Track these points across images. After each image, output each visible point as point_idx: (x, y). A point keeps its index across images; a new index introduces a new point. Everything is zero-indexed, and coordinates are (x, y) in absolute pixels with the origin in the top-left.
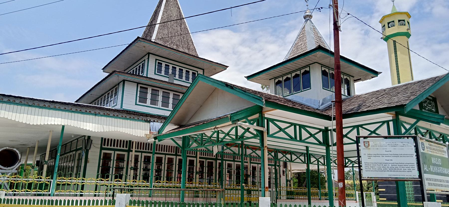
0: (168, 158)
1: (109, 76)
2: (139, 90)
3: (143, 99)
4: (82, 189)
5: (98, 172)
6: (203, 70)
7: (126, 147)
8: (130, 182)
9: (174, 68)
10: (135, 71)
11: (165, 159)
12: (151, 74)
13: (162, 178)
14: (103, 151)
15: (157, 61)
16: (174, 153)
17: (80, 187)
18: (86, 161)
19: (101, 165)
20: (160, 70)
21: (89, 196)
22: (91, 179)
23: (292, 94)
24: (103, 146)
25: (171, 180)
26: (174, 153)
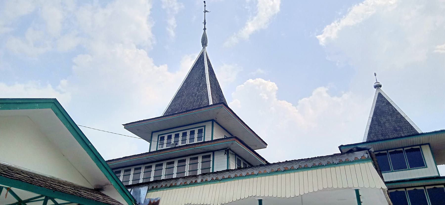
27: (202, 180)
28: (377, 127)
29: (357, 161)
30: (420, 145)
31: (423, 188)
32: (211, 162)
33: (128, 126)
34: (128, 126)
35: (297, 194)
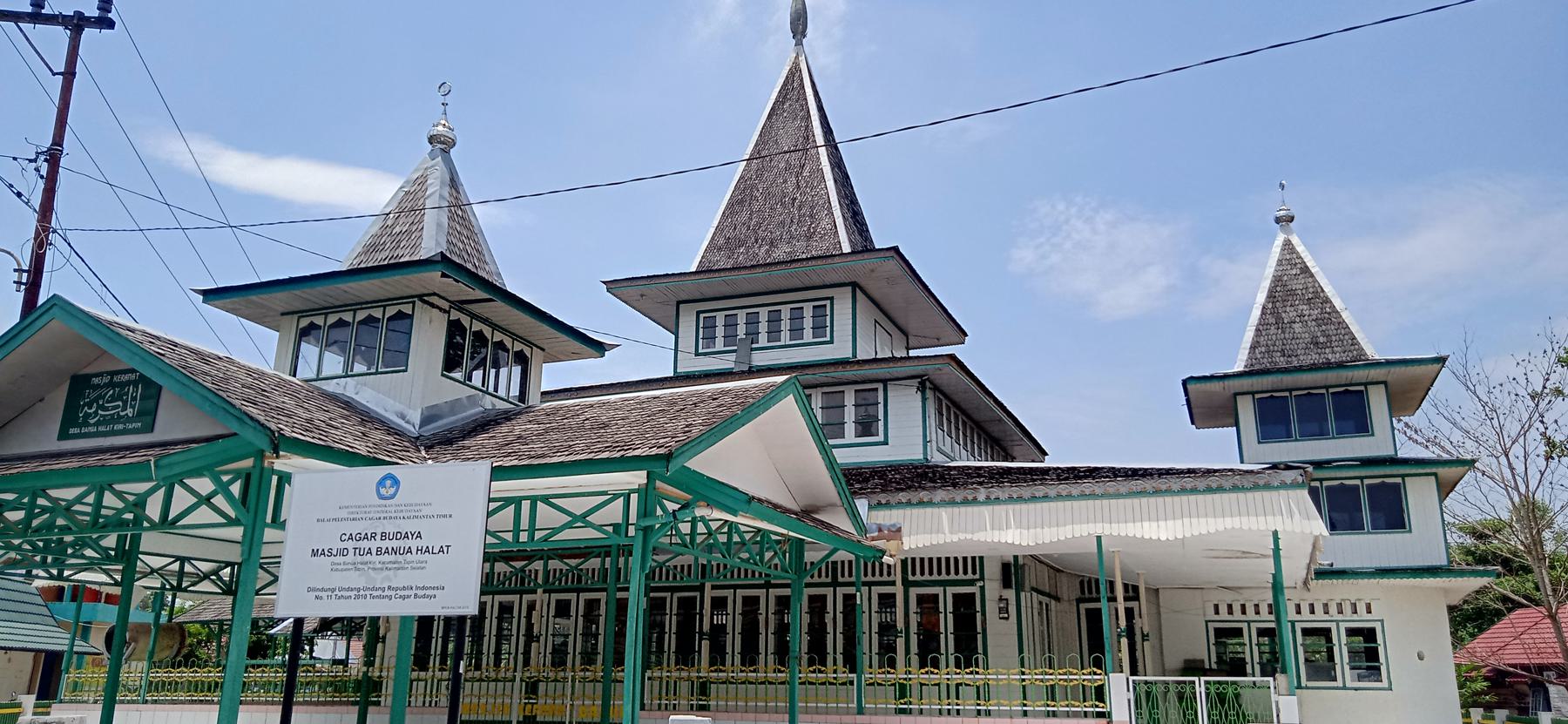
0: (558, 602)
13: (830, 659)
16: (829, 580)
19: (979, 637)
23: (377, 373)
24: (911, 578)
25: (753, 662)
26: (829, 580)
27: (988, 498)
28: (1273, 330)
29: (1283, 486)
30: (1366, 384)
31: (1358, 482)
32: (881, 407)
33: (612, 285)
34: (612, 285)
35: (1180, 536)
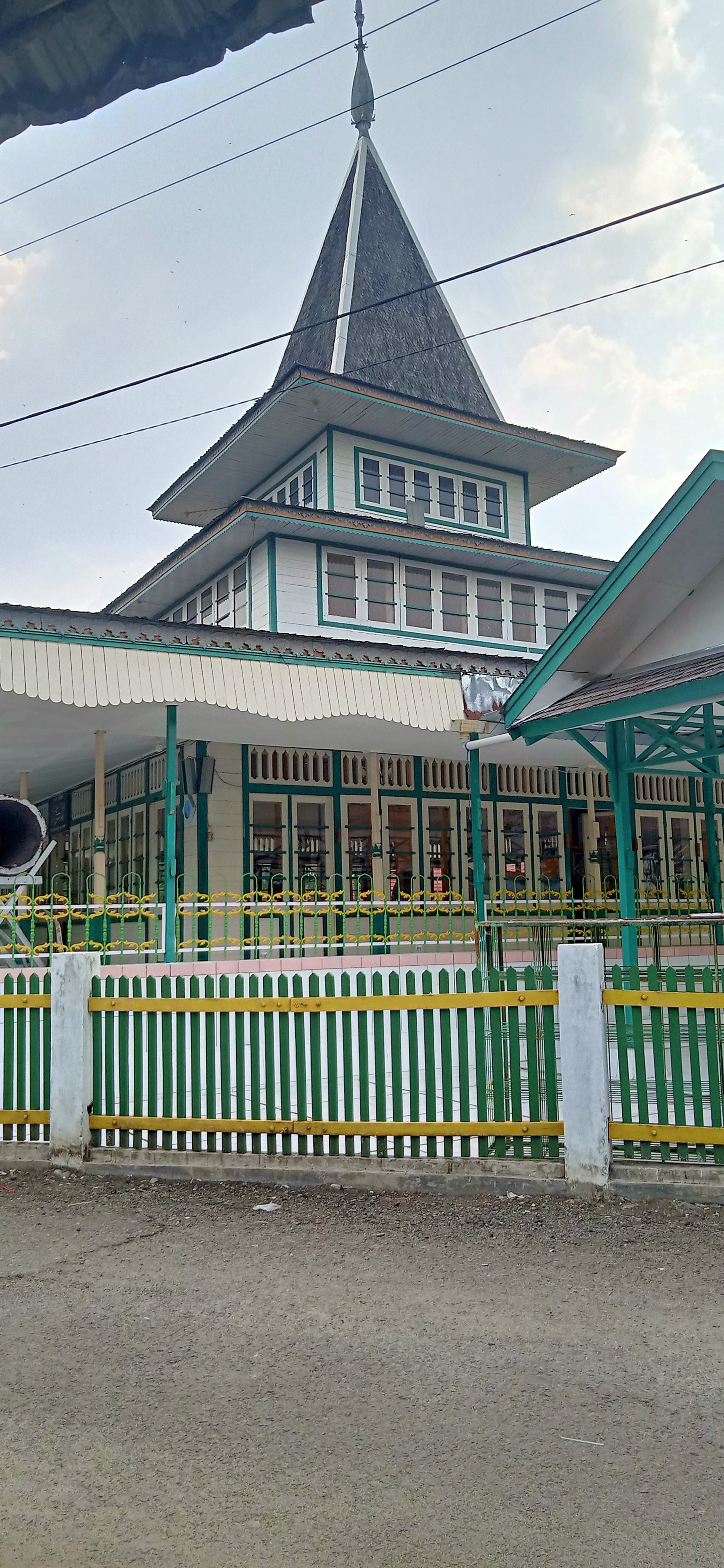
1: (543, 657)
2: (325, 568)
3: (343, 602)
4: (203, 931)
5: (246, 869)
6: (525, 475)
7: (326, 779)
8: (381, 902)
9: (422, 478)
10: (288, 493)
11: (459, 813)
12: (345, 504)
14: (254, 797)
15: (362, 456)
17: (191, 928)
18: (204, 837)
20: (373, 491)
21: (225, 956)
22: (227, 902)
24: (251, 780)
